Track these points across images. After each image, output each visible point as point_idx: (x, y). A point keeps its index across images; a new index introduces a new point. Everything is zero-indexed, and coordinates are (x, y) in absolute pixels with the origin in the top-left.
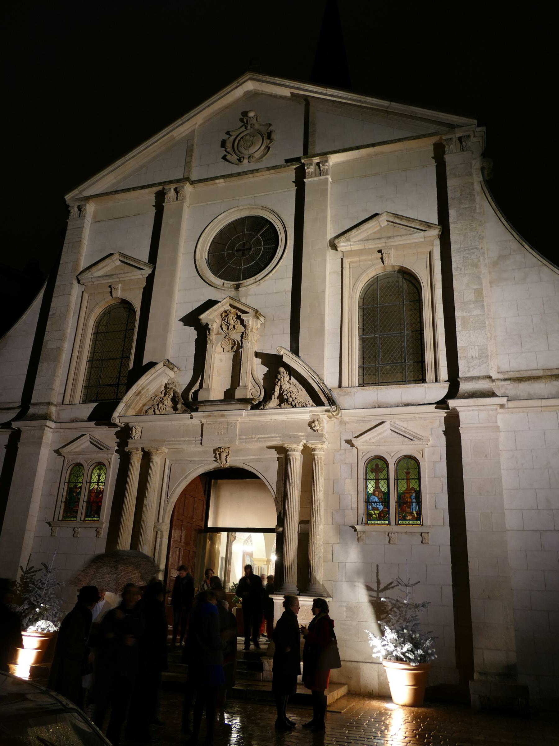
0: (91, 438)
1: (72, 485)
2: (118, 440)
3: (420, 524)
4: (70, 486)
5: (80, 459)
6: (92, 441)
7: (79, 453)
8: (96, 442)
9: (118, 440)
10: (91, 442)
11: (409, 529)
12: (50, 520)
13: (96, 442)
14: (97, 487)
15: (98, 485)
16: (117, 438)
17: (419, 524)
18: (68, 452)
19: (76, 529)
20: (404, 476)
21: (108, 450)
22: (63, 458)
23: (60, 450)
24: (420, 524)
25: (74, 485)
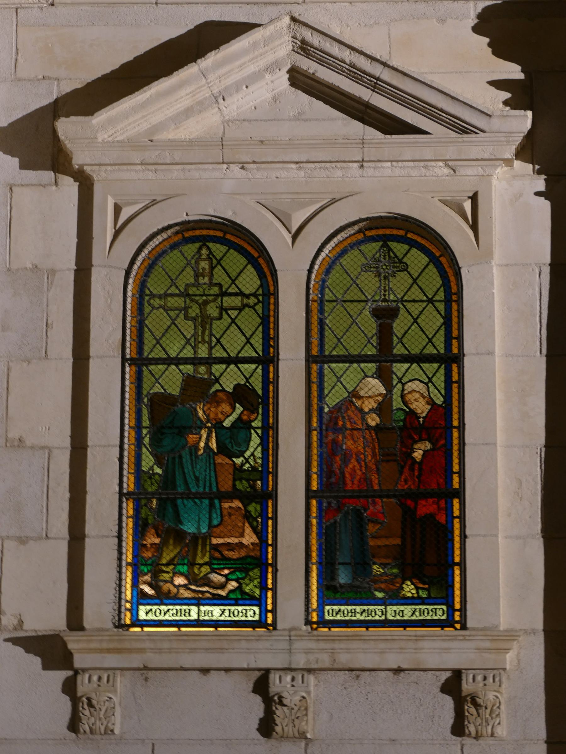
0: (304, 48)
1: (171, 381)
2: (513, 71)
3: (260, 624)
4: (151, 387)
5: (223, 196)
6: (308, 65)
7: (222, 149)
8: (355, 74)
9: (513, 71)
10: (299, 80)
11: (390, 649)
12: (49, 617)
13: (355, 74)
14: (375, 386)
15: (384, 375)
16: (500, 50)
17: (441, 624)
18: (132, 144)
19: (279, 684)
20: (361, 335)
21: (463, 128)
22: (70, 188)
23: (67, 128)
24: (260, 624)
25: (189, 382)
